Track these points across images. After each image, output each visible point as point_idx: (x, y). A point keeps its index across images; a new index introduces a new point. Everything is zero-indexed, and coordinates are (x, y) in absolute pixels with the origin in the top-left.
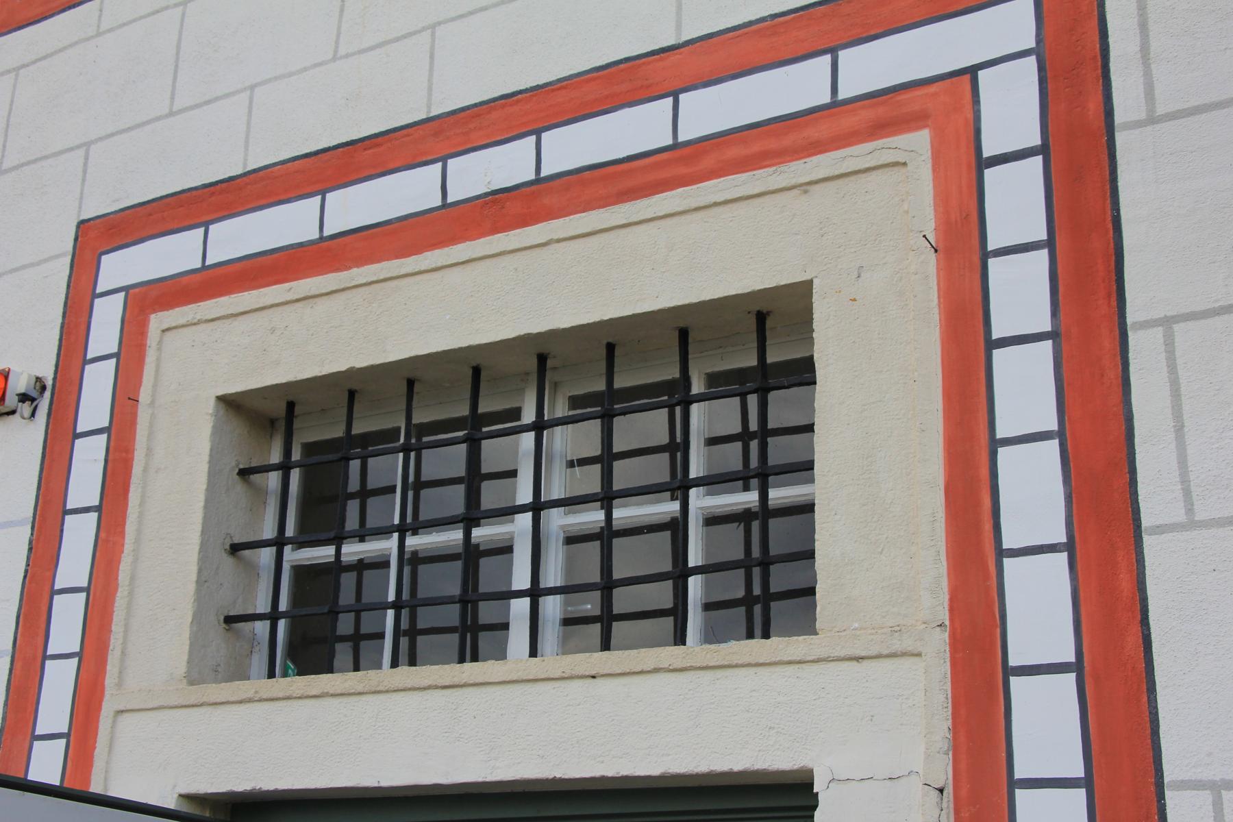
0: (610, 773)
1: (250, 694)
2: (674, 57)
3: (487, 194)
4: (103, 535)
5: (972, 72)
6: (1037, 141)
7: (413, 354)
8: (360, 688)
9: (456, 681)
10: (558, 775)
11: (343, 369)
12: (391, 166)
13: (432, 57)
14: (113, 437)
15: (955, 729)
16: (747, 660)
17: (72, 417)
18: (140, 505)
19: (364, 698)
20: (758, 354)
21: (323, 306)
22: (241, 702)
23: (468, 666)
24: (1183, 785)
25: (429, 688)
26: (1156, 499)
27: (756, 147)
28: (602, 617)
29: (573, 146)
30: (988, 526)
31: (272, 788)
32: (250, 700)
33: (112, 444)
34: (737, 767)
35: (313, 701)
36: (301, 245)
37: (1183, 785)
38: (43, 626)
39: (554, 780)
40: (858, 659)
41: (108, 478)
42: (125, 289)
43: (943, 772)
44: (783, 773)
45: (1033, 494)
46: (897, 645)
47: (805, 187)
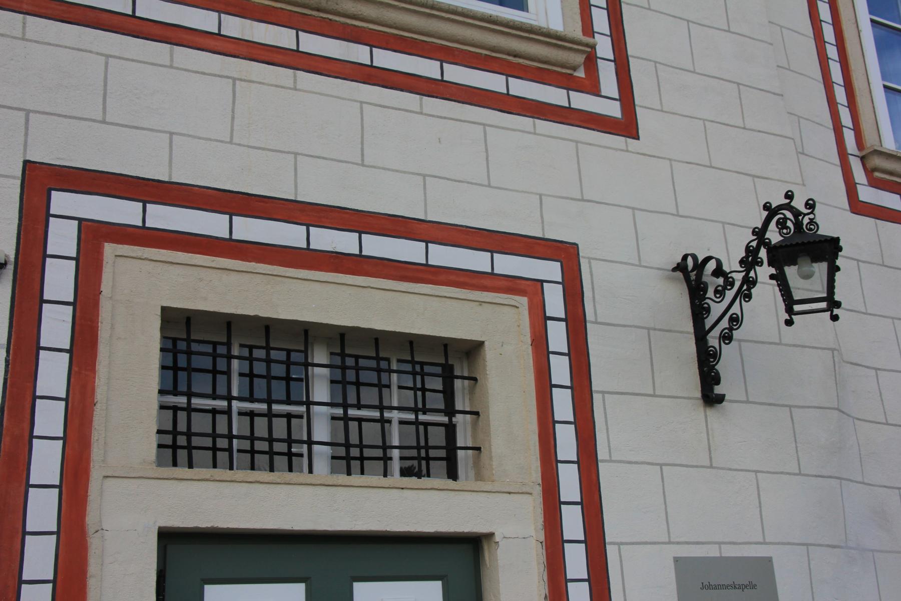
0: (412, 530)
1: (208, 477)
2: (424, 225)
3: (332, 252)
4: (75, 369)
5: (542, 282)
6: (311, 247)
7: (295, 318)
8: (279, 481)
9: (335, 483)
10: (354, 529)
11: (252, 314)
12: (275, 217)
13: (296, 169)
14: (78, 310)
15: (545, 521)
16: (469, 488)
17: (38, 287)
18: (109, 357)
19: (280, 486)
20: (448, 364)
21: (234, 277)
22: (199, 480)
23: (479, 483)
24: (611, 543)
25: (321, 485)
26: (602, 453)
27: (462, 279)
28: (352, 457)
29: (377, 246)
30: (553, 451)
31: (225, 527)
32: (207, 480)
33: (78, 314)
34: (466, 530)
35: (247, 485)
36: (217, 238)
37: (611, 543)
38: (28, 416)
39: (386, 531)
40: (510, 493)
41: (76, 335)
42: (80, 220)
43: (542, 537)
44: (441, 533)
45: (566, 442)
46: (524, 490)
47: (481, 303)
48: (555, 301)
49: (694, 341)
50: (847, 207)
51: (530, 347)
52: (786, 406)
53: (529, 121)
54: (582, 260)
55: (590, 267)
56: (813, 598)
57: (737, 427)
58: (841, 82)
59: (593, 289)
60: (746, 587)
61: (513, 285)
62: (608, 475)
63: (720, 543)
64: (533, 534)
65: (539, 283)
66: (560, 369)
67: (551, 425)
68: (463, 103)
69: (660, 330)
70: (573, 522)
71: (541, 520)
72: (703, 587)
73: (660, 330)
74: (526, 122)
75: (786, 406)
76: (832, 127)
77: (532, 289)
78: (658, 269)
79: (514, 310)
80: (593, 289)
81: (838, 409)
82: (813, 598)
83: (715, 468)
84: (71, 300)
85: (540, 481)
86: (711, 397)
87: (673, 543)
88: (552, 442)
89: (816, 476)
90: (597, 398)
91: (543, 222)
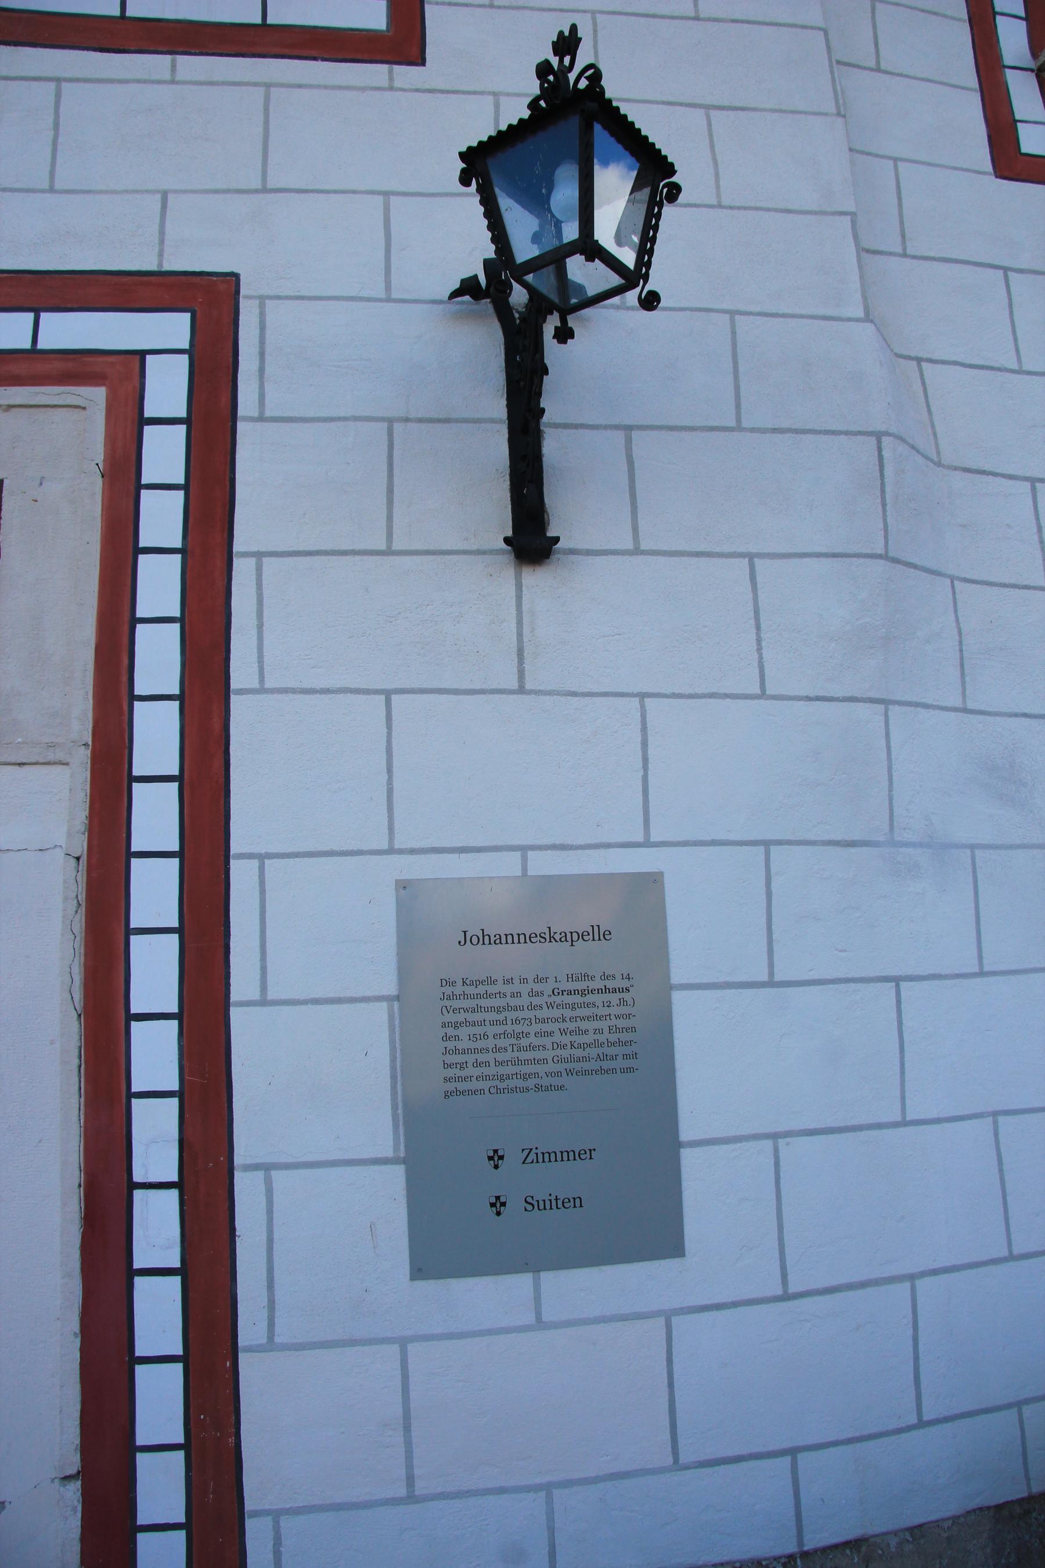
5: (142, 354)
15: (91, 817)
40: (20, 764)
43: (80, 846)
46: (51, 756)
48: (167, 388)
49: (507, 436)
50: (988, 166)
51: (99, 482)
52: (741, 555)
53: (162, 61)
54: (243, 304)
55: (262, 315)
56: (4, 190)
57: (593, 609)
58: (1011, 76)
59: (262, 355)
60: (581, 936)
61: (76, 367)
62: (251, 724)
63: (524, 849)
64: (62, 841)
65: (137, 358)
66: (162, 518)
67: (126, 628)
68: (16, 44)
69: (420, 421)
70: (155, 817)
71: (82, 814)
72: (466, 939)
73: (420, 421)
74: (157, 64)
75: (741, 555)
76: (966, 17)
77: (121, 374)
78: (589, 553)
79: (76, 414)
80: (262, 355)
81: (885, 557)
82: (4, 190)
83: (530, 692)
84: (134, 861)
85: (89, 739)
86: (531, 539)
87: (401, 852)
88: (126, 661)
89: (809, 699)
90: (242, 571)
91: (162, 242)
